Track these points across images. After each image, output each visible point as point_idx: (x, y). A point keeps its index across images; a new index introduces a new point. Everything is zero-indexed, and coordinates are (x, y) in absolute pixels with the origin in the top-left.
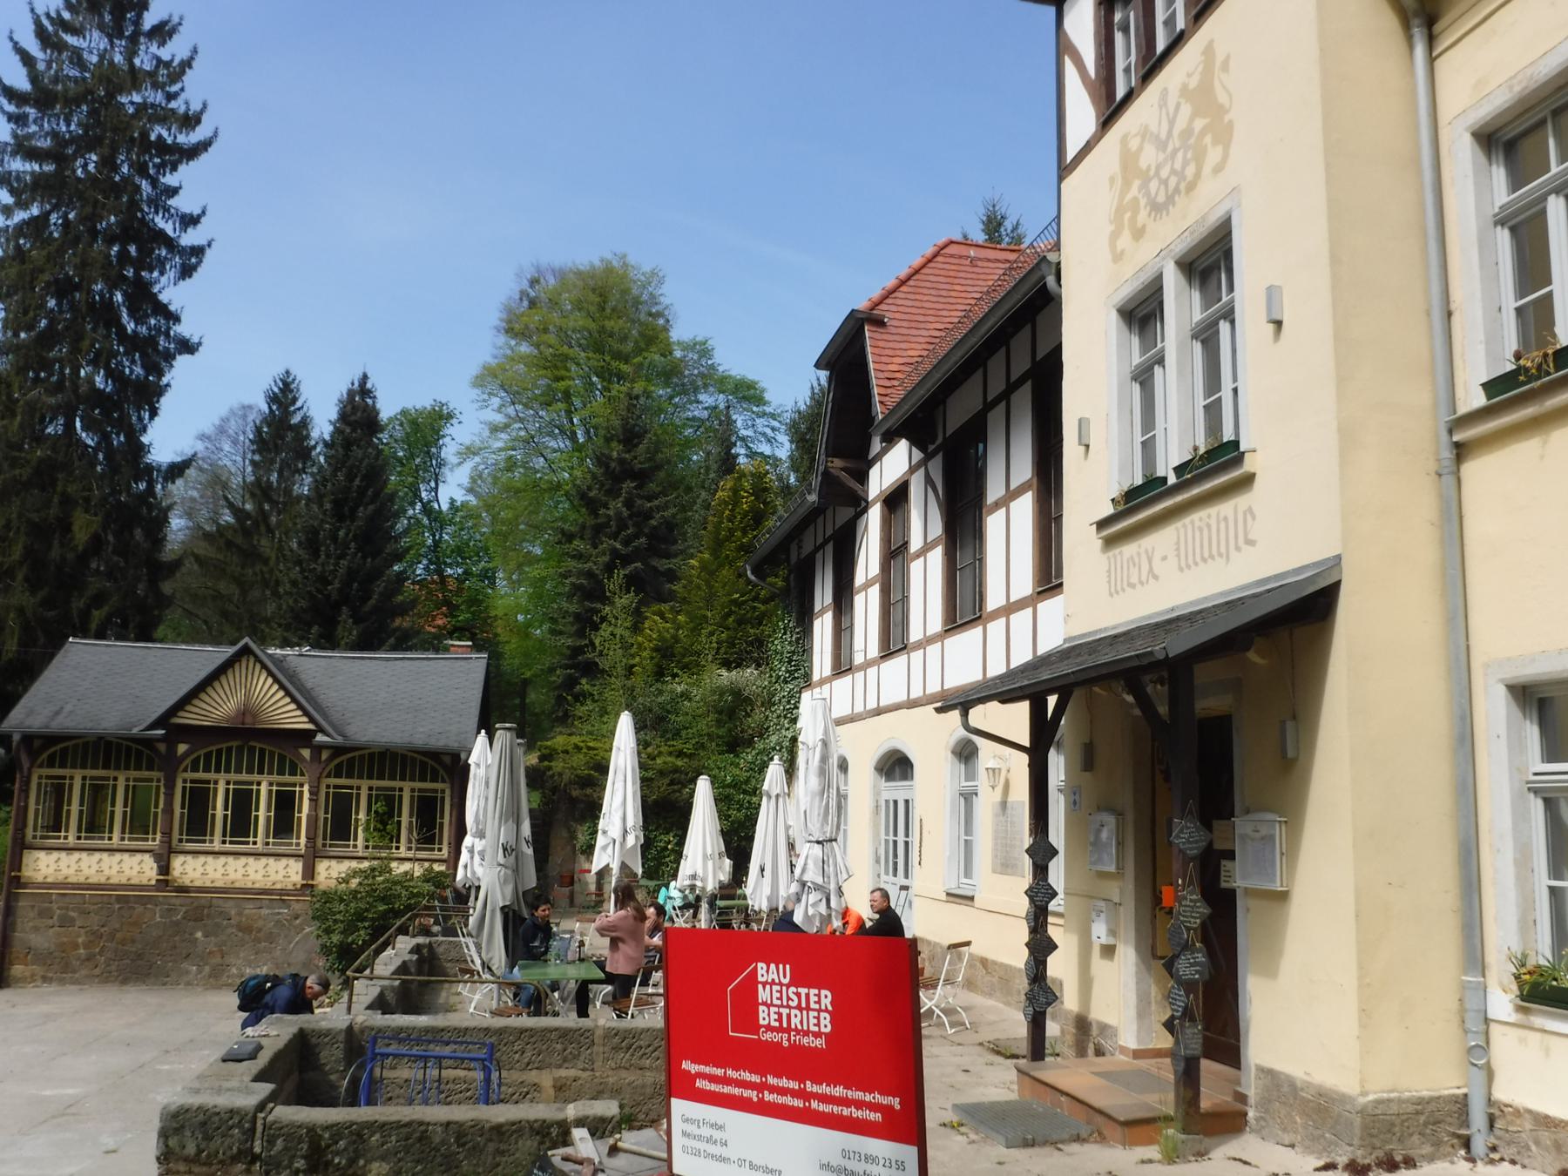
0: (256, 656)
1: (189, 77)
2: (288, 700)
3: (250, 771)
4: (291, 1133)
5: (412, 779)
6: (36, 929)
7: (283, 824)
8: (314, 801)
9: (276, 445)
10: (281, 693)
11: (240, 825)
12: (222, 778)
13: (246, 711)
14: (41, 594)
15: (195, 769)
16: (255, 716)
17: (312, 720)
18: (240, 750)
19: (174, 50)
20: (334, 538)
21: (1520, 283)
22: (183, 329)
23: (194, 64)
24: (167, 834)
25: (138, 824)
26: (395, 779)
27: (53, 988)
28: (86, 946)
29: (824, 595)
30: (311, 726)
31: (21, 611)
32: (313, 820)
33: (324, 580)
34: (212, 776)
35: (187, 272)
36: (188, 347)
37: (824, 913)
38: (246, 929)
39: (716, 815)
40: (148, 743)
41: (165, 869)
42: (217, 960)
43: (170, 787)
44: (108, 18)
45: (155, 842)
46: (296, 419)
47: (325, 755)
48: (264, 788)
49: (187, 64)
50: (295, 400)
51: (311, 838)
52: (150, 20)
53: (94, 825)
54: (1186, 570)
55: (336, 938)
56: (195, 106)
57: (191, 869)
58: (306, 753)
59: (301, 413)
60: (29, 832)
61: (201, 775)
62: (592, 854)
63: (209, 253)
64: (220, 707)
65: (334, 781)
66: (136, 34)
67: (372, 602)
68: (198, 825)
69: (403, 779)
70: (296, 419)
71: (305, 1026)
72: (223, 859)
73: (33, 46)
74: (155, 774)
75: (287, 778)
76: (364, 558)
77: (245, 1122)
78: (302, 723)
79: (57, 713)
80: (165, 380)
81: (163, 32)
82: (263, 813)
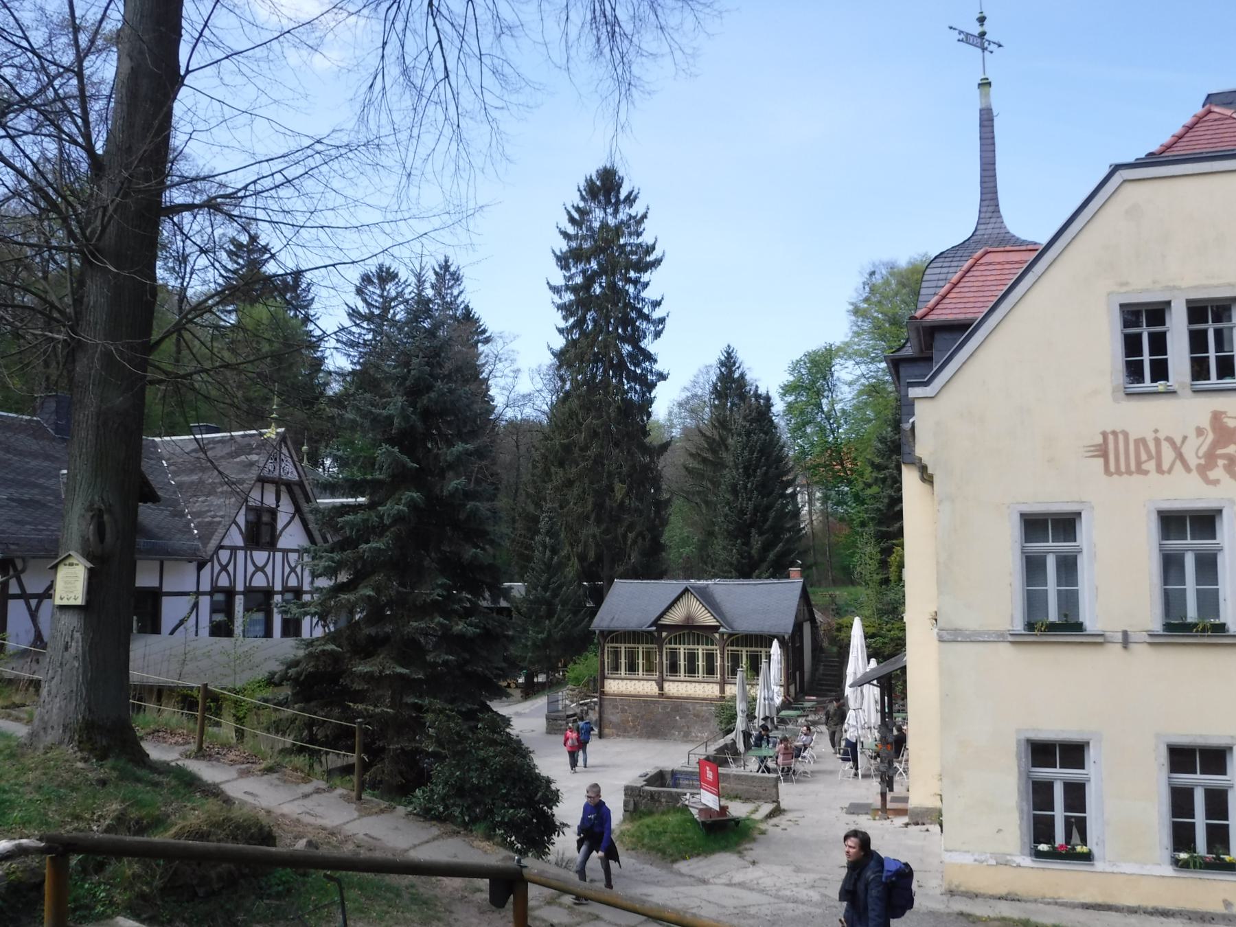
1: (646, 224)
4: (647, 791)
6: (612, 714)
7: (710, 670)
8: (722, 658)
9: (726, 395)
11: (692, 670)
12: (682, 647)
13: (689, 618)
14: (603, 527)
15: (670, 643)
16: (693, 619)
18: (689, 634)
19: (637, 209)
20: (745, 487)
21: (1027, 568)
22: (657, 367)
23: (648, 215)
24: (662, 672)
25: (649, 669)
27: (621, 739)
28: (633, 721)
31: (594, 536)
32: (723, 667)
33: (742, 512)
34: (677, 646)
35: (657, 334)
36: (662, 377)
38: (697, 716)
40: (650, 633)
41: (661, 688)
42: (686, 729)
43: (661, 652)
44: (601, 198)
45: (656, 676)
46: (736, 375)
47: (725, 637)
48: (682, 651)
49: (645, 216)
50: (735, 363)
51: (723, 675)
52: (623, 194)
53: (632, 668)
55: (723, 726)
56: (650, 242)
57: (672, 688)
58: (717, 636)
59: (741, 369)
60: (606, 672)
61: (673, 646)
63: (667, 321)
64: (676, 616)
65: (730, 648)
66: (618, 202)
67: (768, 523)
68: (674, 668)
70: (736, 375)
72: (685, 684)
73: (571, 230)
74: (654, 646)
75: (710, 647)
76: (763, 498)
77: (639, 789)
78: (713, 622)
79: (613, 619)
80: (653, 395)
81: (630, 200)
82: (701, 663)
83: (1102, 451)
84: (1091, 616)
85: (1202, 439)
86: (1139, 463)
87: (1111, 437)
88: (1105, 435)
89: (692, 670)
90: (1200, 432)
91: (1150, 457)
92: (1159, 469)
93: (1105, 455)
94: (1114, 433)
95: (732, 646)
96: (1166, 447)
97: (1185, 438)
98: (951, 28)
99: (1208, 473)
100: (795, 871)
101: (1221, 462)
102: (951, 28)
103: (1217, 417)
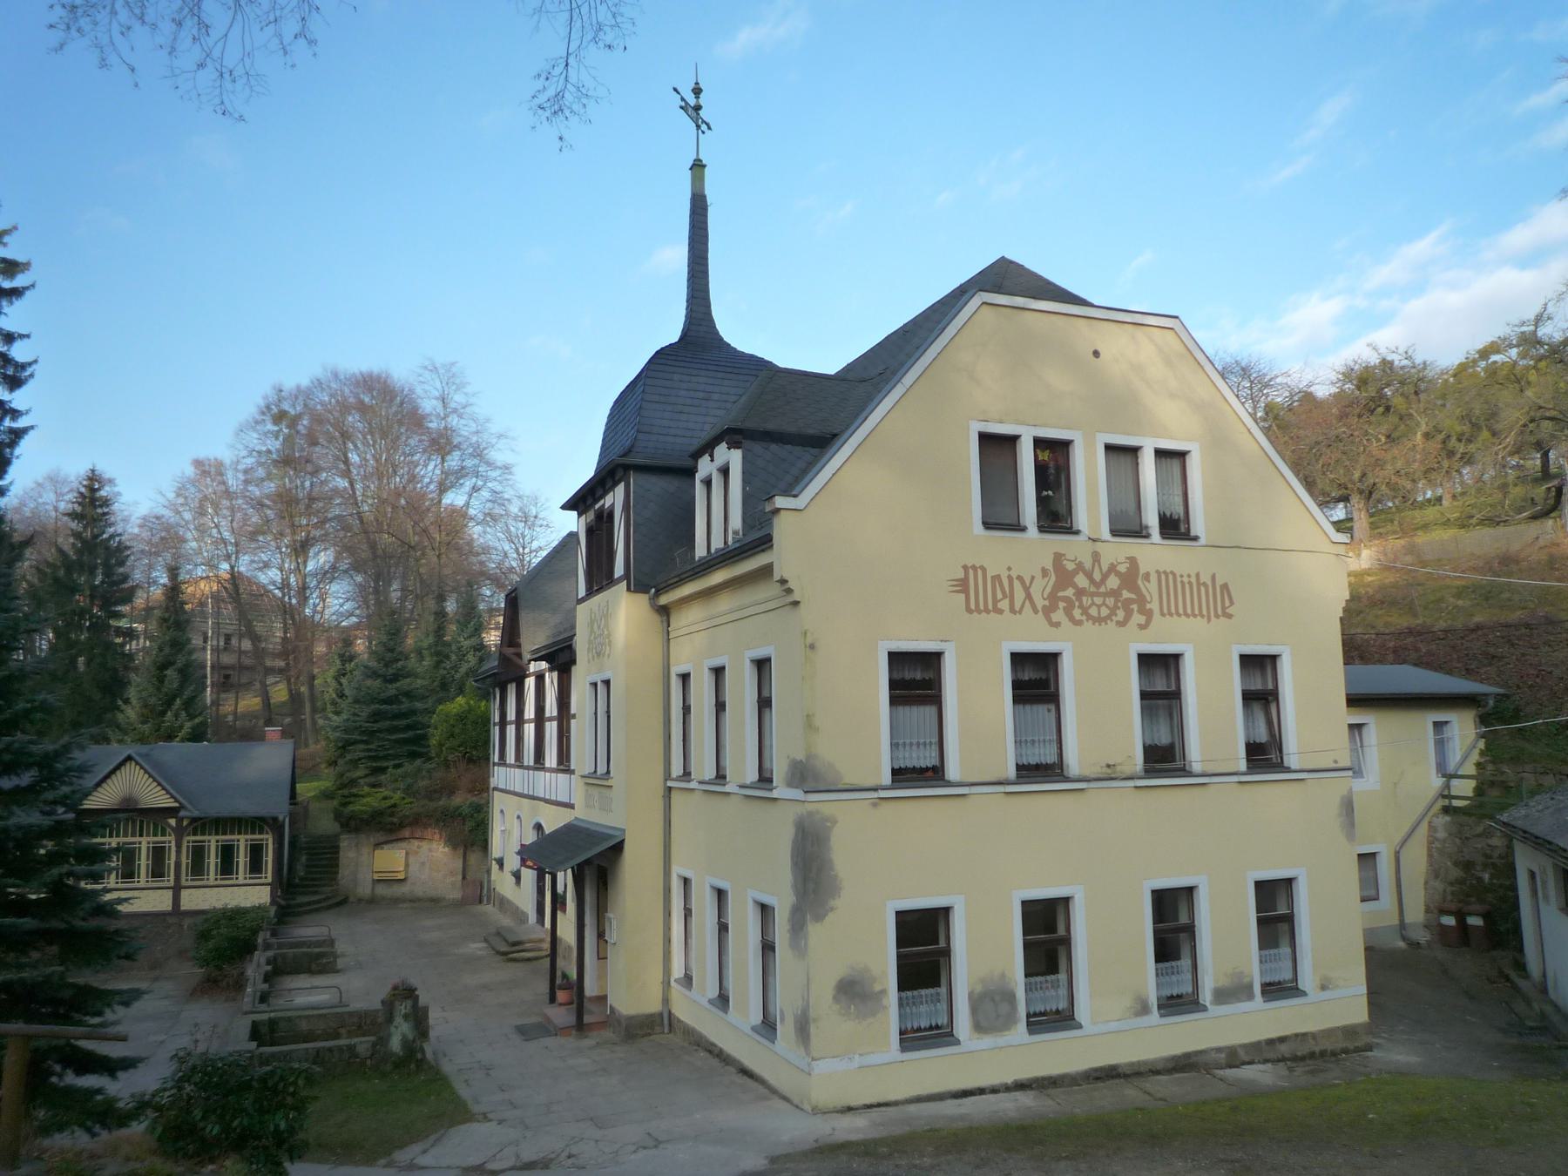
0: (135, 760)
2: (155, 784)
3: (133, 835)
5: (246, 833)
7: (157, 871)
8: (178, 852)
10: (151, 780)
11: (227, 867)
17: (177, 801)
26: (234, 834)
29: (492, 697)
30: (177, 805)
32: (178, 865)
37: (344, 468)
39: (236, 815)
54: (796, 596)
62: (589, 859)
69: (240, 833)
71: (255, 1019)
75: (159, 838)
78: (165, 802)
83: (962, 586)
84: (1074, 762)
85: (1046, 579)
86: (995, 601)
87: (971, 572)
88: (965, 568)
89: (227, 867)
90: (1045, 572)
91: (1005, 596)
92: (1013, 610)
93: (965, 591)
94: (974, 568)
95: (195, 834)
96: (1017, 583)
97: (1033, 578)
98: (675, 90)
99: (1052, 615)
100: (499, 1124)
101: (1062, 605)
102: (675, 90)
103: (1058, 558)
